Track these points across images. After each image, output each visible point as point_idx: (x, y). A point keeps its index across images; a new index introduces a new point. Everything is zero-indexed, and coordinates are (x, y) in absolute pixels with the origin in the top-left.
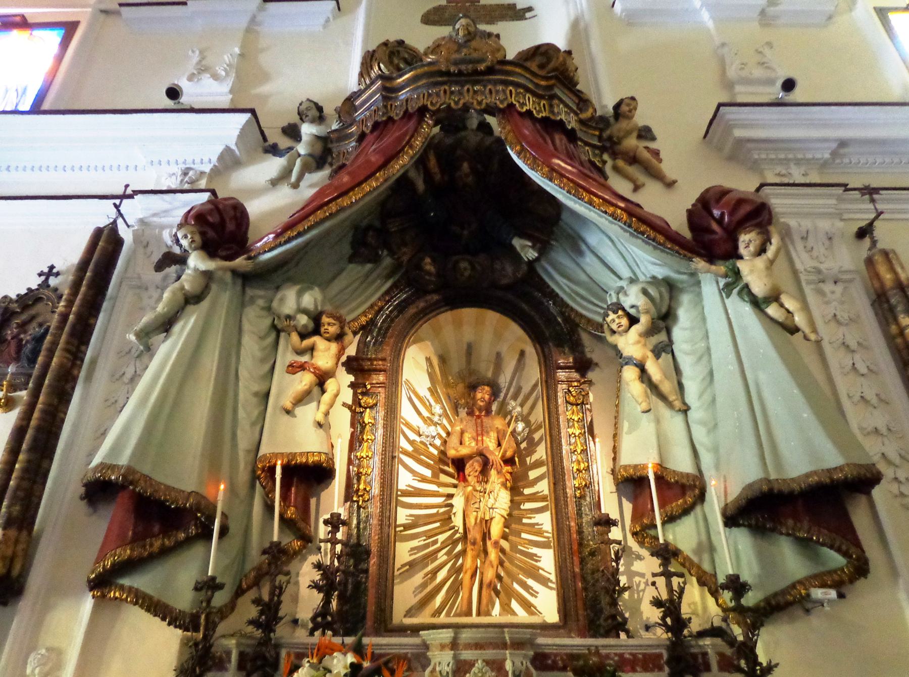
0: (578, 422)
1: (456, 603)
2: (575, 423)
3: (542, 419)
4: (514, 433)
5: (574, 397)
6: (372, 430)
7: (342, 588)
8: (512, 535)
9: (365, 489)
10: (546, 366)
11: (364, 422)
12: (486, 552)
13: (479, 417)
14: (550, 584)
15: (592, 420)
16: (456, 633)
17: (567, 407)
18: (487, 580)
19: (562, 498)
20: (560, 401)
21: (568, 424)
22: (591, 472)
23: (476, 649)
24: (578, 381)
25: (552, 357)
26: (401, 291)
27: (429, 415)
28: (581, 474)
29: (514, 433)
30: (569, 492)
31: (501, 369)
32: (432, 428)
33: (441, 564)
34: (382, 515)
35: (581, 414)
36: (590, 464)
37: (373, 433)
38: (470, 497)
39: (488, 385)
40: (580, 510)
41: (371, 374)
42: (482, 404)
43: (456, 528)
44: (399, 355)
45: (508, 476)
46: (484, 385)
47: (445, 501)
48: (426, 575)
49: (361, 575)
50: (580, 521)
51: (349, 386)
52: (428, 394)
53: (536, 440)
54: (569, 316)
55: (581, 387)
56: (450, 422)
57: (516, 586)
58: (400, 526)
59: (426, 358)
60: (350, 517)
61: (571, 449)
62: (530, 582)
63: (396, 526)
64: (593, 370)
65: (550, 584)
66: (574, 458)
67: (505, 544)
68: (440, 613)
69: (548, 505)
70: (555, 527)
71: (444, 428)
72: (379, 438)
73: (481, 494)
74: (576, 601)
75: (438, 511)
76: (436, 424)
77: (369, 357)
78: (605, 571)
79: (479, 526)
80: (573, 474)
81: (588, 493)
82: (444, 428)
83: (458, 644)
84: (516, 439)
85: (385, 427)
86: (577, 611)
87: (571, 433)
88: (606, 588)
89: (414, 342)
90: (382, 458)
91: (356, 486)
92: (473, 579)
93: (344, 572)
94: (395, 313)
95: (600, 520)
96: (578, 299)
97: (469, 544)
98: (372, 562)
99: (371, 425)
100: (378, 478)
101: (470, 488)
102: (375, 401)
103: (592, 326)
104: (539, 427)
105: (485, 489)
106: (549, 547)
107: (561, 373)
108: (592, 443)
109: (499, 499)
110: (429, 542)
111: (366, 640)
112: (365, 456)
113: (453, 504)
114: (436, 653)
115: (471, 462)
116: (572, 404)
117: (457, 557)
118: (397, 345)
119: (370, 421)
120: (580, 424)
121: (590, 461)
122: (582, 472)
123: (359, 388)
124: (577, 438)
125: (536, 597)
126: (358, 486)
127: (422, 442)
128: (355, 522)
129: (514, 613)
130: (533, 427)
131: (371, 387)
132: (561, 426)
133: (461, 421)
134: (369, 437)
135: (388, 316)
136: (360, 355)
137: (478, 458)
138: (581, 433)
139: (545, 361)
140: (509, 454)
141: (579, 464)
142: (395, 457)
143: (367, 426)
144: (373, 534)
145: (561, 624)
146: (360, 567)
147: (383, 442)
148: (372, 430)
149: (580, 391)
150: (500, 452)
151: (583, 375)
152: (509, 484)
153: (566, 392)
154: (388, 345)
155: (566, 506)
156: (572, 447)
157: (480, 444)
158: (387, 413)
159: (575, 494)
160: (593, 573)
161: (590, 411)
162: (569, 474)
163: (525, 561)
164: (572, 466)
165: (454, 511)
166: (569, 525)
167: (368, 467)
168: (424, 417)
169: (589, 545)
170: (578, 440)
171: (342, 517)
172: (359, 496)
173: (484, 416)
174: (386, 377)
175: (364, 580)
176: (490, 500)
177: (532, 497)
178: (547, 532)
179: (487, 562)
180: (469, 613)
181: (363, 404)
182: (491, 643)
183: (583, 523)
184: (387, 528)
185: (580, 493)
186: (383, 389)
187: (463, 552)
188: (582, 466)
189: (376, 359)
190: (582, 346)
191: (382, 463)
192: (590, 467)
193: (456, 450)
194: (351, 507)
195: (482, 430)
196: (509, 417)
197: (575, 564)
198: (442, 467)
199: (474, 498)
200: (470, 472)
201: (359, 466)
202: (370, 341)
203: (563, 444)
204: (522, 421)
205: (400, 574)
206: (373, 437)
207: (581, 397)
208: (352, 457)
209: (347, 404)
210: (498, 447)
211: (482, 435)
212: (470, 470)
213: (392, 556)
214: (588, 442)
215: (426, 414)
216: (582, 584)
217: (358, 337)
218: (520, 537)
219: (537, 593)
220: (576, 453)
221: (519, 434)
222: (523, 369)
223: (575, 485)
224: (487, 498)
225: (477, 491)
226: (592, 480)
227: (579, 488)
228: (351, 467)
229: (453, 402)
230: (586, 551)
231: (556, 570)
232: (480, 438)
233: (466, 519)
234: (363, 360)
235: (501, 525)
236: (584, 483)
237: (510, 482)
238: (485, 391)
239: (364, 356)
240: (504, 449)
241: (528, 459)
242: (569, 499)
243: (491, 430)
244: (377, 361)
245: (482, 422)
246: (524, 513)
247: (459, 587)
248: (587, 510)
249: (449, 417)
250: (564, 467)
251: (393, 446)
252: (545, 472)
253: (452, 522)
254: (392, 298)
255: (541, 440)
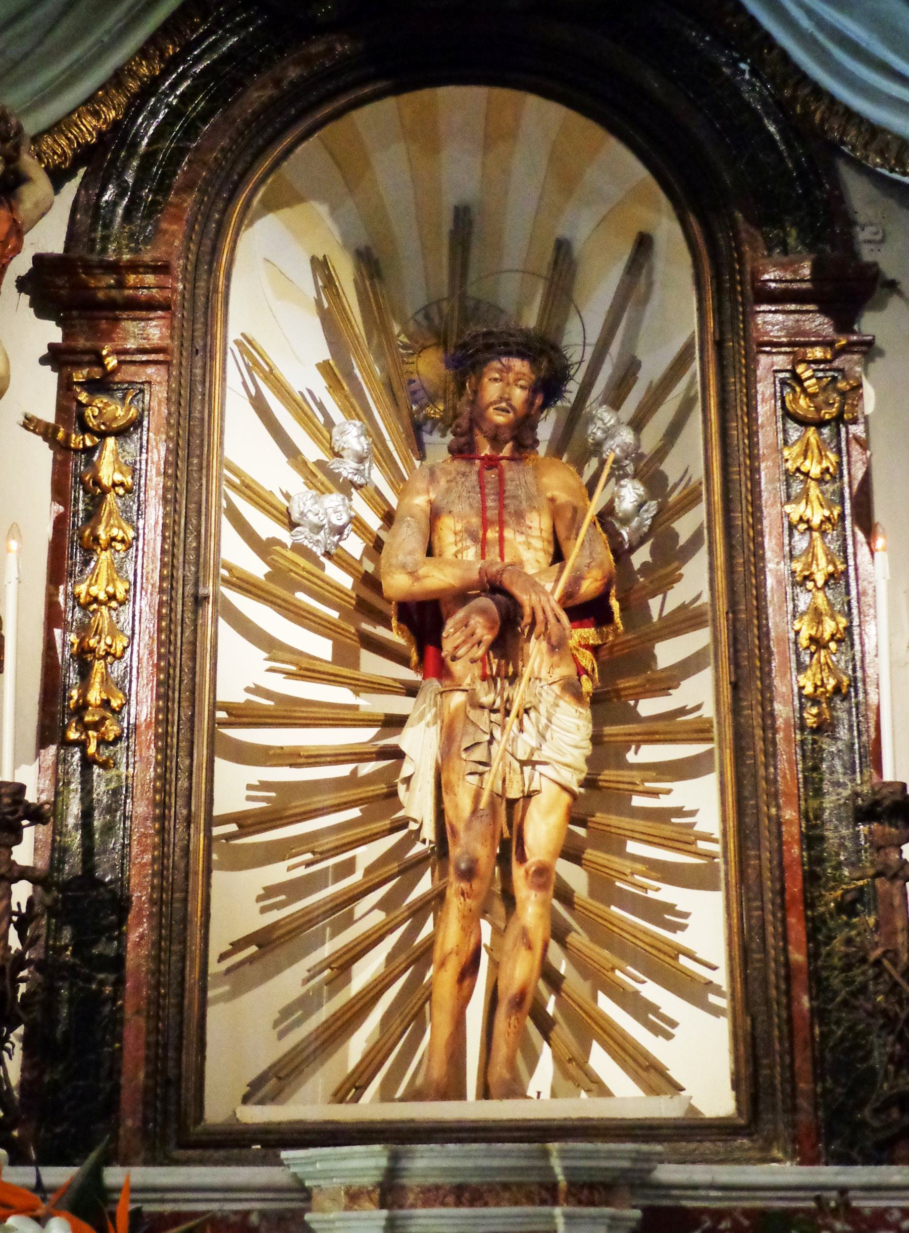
0: (820, 481)
1: (408, 1064)
2: (812, 484)
3: (702, 473)
4: (606, 516)
5: (812, 396)
6: (126, 509)
7: (37, 1014)
8: (596, 847)
9: (106, 703)
10: (719, 291)
11: (97, 482)
12: (509, 899)
13: (491, 463)
14: (713, 999)
15: (867, 476)
16: (394, 1157)
17: (785, 431)
18: (511, 985)
19: (759, 732)
20: (764, 410)
21: (788, 486)
22: (857, 647)
23: (459, 1203)
24: (827, 344)
25: (741, 260)
26: (218, 24)
27: (323, 456)
28: (823, 652)
29: (606, 516)
30: (782, 710)
31: (571, 300)
32: (334, 500)
33: (366, 936)
34: (164, 786)
35: (833, 457)
36: (856, 622)
37: (128, 520)
38: (459, 726)
39: (521, 355)
40: (816, 768)
41: (117, 320)
42: (500, 419)
43: (413, 826)
44: (215, 251)
45: (587, 659)
46: (509, 354)
47: (377, 738)
48: (314, 972)
49: (101, 976)
50: (814, 804)
51: (43, 361)
52: (320, 386)
53: (682, 541)
54: (807, 115)
55: (836, 364)
56: (397, 480)
57: (606, 1005)
58: (226, 819)
59: (314, 260)
60: (57, 794)
61: (793, 573)
62: (652, 991)
63: (211, 821)
64: (880, 306)
65: (713, 999)
66: (804, 601)
67: (568, 872)
68: (361, 1089)
69: (710, 752)
70: (731, 823)
71: (376, 499)
72: (150, 536)
73: (496, 717)
74: (791, 1052)
75: (354, 772)
76: (346, 487)
77: (112, 258)
78: (886, 963)
79: (486, 820)
80: (798, 655)
81: (844, 716)
82: (376, 499)
83: (403, 1188)
84: (613, 536)
85: (169, 499)
86: (792, 1080)
87: (795, 518)
88: (884, 1013)
89: (269, 206)
90: (161, 604)
91: (75, 693)
92: (466, 983)
93: (40, 966)
94: (200, 103)
95: (876, 803)
96: (839, 55)
97: (452, 876)
98: (133, 937)
99: (121, 491)
100: (147, 670)
101: (458, 699)
102: (133, 412)
103: (881, 153)
104: (690, 501)
105: (509, 700)
106: (713, 886)
107: (770, 317)
108: (864, 550)
109: (556, 734)
110: (327, 868)
111: (114, 1176)
112: (102, 596)
113: (404, 748)
114: (332, 1216)
115: (460, 614)
116: (803, 422)
117: (419, 912)
118: (208, 217)
119: (118, 478)
120: (829, 487)
121: (855, 611)
122: (826, 647)
123: (79, 365)
124: (816, 534)
125: (669, 1036)
126: (83, 695)
127: (298, 548)
128: (75, 808)
129: (600, 1089)
130: (672, 499)
131: (120, 363)
132: (765, 495)
133: (432, 476)
134: (115, 532)
135: (175, 114)
136: (80, 251)
137: (485, 602)
138: (828, 519)
139: (717, 277)
140: (589, 587)
141: (820, 623)
142: (206, 598)
143: (110, 497)
144: (135, 850)
145: (742, 1122)
146: (95, 951)
147: (163, 551)
148: (126, 509)
149: (834, 379)
150: (557, 581)
151: (844, 324)
152: (587, 686)
153: (783, 382)
154: (177, 219)
155: (771, 755)
156: (798, 566)
157: (493, 554)
158: (173, 452)
159: (802, 718)
160: (848, 968)
161: (864, 445)
162: (783, 654)
163: (634, 926)
164: (797, 626)
165: (406, 770)
166: (778, 817)
167: (114, 632)
168: (305, 463)
169: (839, 880)
170: (818, 543)
171: (31, 797)
172: (85, 727)
173: (511, 459)
174: (172, 328)
175: (108, 990)
176: (524, 736)
177: (660, 726)
178: (708, 838)
179: (513, 932)
180: (460, 1095)
181: (93, 423)
182: (506, 1186)
183: (822, 810)
184: (181, 827)
185: (818, 715)
186: (163, 369)
187: (437, 900)
188: (829, 627)
189: (134, 267)
190: (850, 223)
191: (160, 617)
192: (856, 631)
193: (412, 574)
194: (60, 761)
195: (502, 507)
196: (594, 463)
197: (792, 935)
198: (366, 627)
199: (471, 729)
200: (456, 648)
201: (84, 629)
202: (114, 204)
203: (768, 554)
204: (635, 476)
205: (229, 971)
206: (131, 534)
207: (835, 397)
208: (61, 599)
209: (39, 421)
210: (553, 563)
211: (502, 524)
212: (459, 638)
213: (198, 920)
214: (850, 550)
215: (312, 452)
216: (811, 999)
217: (71, 188)
218: (621, 852)
219: (673, 1024)
220: (810, 585)
221: (625, 521)
222: (645, 300)
223: (801, 688)
224: (515, 729)
225: (482, 707)
226: (859, 674)
227: (815, 701)
228: (57, 632)
229: (405, 413)
230: (831, 897)
231: (731, 958)
232: (492, 534)
233: (446, 799)
234: (89, 268)
235: (557, 817)
236: (831, 683)
237: (591, 678)
238: (511, 377)
239: (95, 258)
240: (576, 569)
241: (654, 604)
242: (779, 736)
243: (533, 508)
244: (136, 272)
245: (501, 480)
246: (636, 776)
247: (422, 1007)
248: (840, 769)
249: (395, 463)
250: (768, 633)
251: (197, 564)
252: (705, 648)
253: (400, 807)
254: (188, 48)
255: (695, 541)
